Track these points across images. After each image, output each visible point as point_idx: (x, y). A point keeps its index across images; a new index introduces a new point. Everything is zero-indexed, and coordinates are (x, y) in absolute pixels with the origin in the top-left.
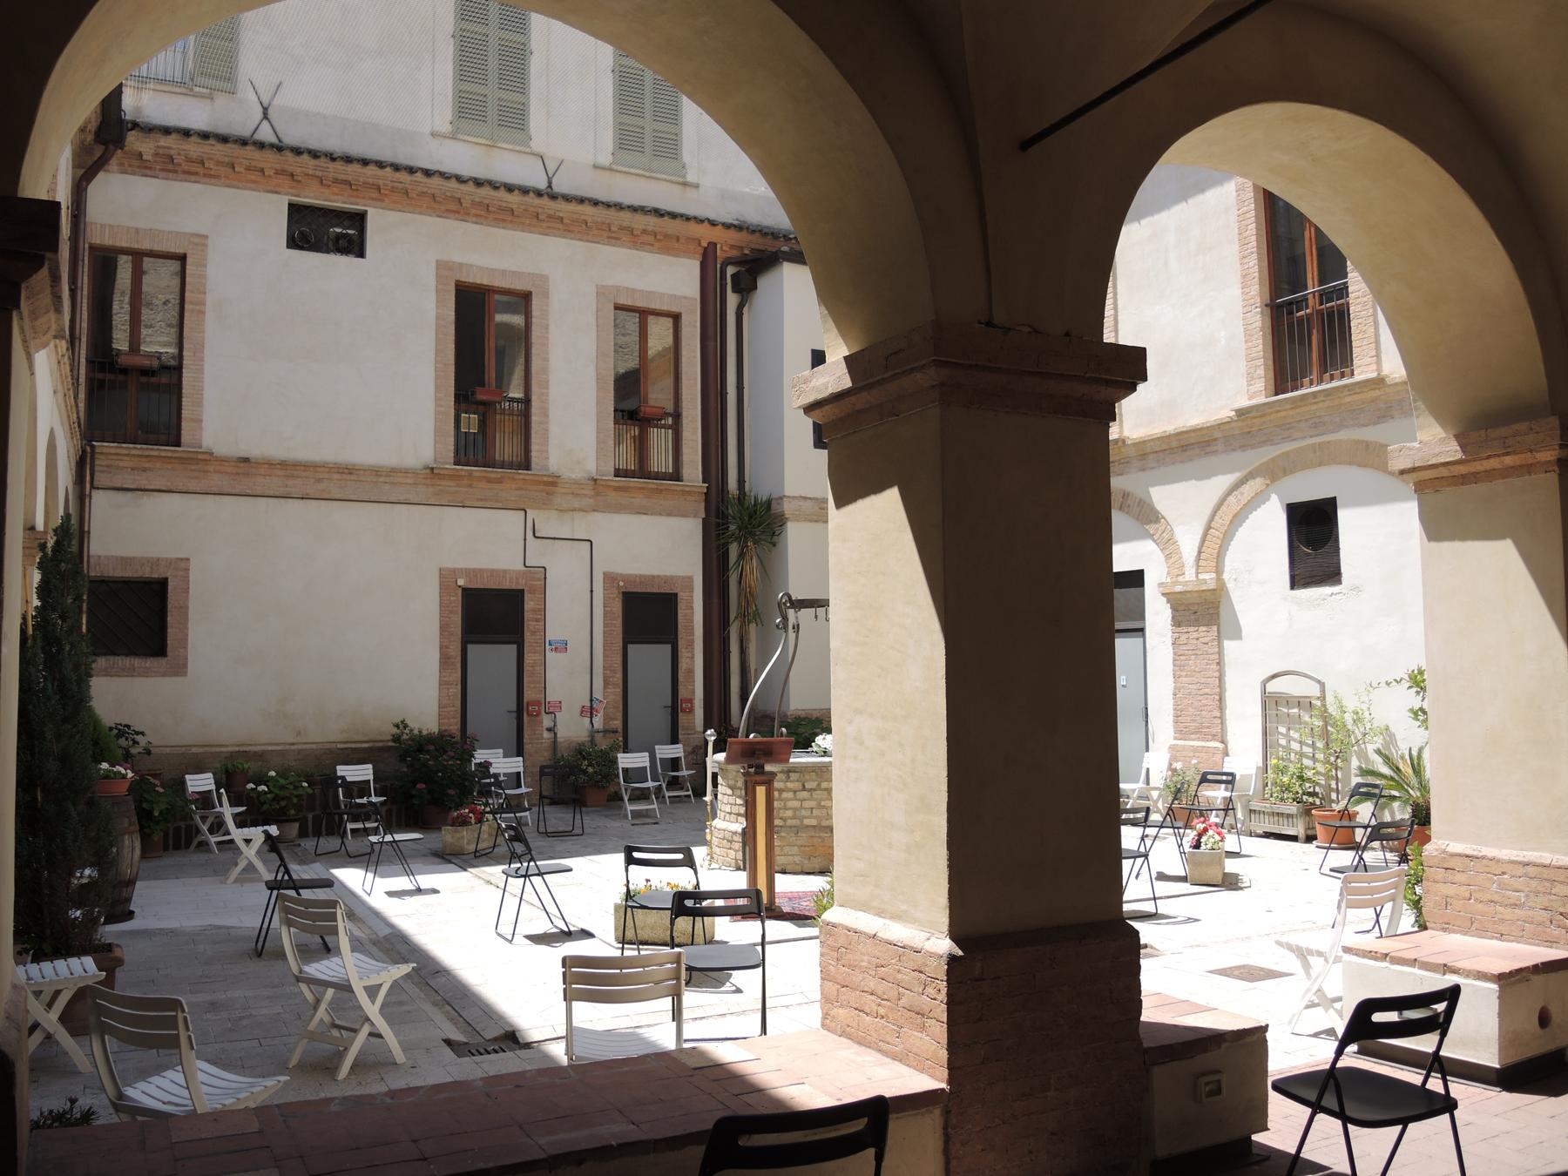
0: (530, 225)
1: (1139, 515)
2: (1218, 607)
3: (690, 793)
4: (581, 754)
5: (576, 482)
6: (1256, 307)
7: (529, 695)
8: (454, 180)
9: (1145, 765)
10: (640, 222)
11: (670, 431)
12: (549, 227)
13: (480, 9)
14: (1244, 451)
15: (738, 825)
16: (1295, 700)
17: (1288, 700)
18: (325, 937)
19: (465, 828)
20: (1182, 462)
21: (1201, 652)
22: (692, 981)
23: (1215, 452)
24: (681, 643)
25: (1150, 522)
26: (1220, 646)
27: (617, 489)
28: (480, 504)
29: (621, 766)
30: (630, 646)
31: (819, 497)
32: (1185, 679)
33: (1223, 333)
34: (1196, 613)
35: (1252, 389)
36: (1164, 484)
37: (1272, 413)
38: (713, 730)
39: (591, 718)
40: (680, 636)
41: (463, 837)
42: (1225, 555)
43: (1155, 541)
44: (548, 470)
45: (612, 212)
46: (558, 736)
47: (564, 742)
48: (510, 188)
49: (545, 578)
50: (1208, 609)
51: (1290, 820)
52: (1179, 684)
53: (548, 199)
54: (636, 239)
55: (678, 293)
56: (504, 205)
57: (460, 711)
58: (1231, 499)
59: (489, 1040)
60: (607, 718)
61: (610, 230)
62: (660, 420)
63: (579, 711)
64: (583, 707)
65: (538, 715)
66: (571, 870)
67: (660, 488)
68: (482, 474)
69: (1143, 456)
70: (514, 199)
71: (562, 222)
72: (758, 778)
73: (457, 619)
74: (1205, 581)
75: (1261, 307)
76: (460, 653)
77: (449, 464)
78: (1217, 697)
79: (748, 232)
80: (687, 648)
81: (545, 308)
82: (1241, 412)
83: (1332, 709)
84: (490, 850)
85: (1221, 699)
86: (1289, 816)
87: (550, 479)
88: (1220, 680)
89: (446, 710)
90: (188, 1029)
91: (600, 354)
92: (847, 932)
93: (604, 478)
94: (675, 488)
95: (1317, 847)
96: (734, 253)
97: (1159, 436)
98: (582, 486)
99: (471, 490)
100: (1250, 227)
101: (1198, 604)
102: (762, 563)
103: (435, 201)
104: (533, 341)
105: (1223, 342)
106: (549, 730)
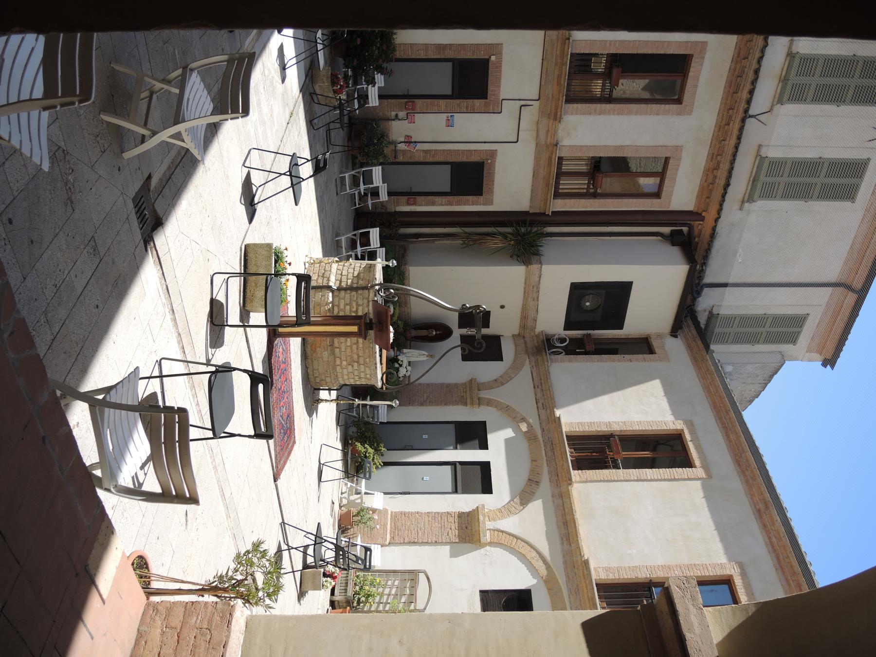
0: (726, 103)
1: (525, 492)
2: (470, 543)
3: (357, 206)
4: (381, 137)
5: (555, 133)
6: (650, 575)
7: (419, 102)
8: (761, 55)
9: (376, 493)
10: (722, 175)
11: (585, 191)
12: (723, 116)
13: (872, 70)
14: (563, 563)
15: (334, 281)
16: (415, 591)
17: (414, 587)
18: (140, 377)
19: (330, 84)
20: (557, 521)
22: (214, 326)
23: (562, 544)
24: (451, 198)
25: (521, 499)
26: (446, 543)
27: (550, 159)
28: (544, 70)
29: (371, 230)
30: (449, 166)
31: (540, 285)
32: (427, 520)
33: (634, 551)
35: (600, 570)
36: (544, 510)
37: (586, 583)
38: (396, 264)
39: (404, 142)
40: (455, 197)
41: (324, 83)
42: (501, 548)
43: (509, 502)
44: (564, 115)
45: (730, 157)
46: (393, 122)
47: (389, 125)
48: (751, 92)
49: (494, 113)
50: (469, 536)
51: (343, 591)
52: (424, 516)
53: (742, 116)
54: (711, 171)
55: (673, 197)
56: (741, 88)
57: (409, 57)
58: (534, 554)
59: (154, 206)
60: (404, 152)
61: (718, 155)
62: (593, 186)
63: (408, 134)
64: (411, 137)
65: (406, 109)
66: (296, 204)
67: (550, 185)
68: (564, 72)
69: (561, 496)
70: (745, 94)
71: (725, 125)
72: (363, 327)
73: (469, 55)
74: (485, 536)
75: (650, 577)
76: (447, 57)
77: (572, 51)
78: (416, 541)
79: (709, 241)
80: (448, 201)
81: (671, 113)
82: (586, 563)
84: (316, 101)
85: (415, 543)
86: (346, 590)
87: (558, 117)
88: (426, 542)
89: (409, 48)
90: (62, 105)
91: (637, 148)
92: (223, 644)
93: (558, 151)
94: (549, 194)
95: (328, 609)
96: (696, 232)
97: (573, 508)
98: (553, 137)
99: (554, 65)
100: (699, 572)
101: (472, 530)
102: (500, 250)
103: (748, 41)
104: (649, 105)
105: (629, 551)
106: (397, 115)
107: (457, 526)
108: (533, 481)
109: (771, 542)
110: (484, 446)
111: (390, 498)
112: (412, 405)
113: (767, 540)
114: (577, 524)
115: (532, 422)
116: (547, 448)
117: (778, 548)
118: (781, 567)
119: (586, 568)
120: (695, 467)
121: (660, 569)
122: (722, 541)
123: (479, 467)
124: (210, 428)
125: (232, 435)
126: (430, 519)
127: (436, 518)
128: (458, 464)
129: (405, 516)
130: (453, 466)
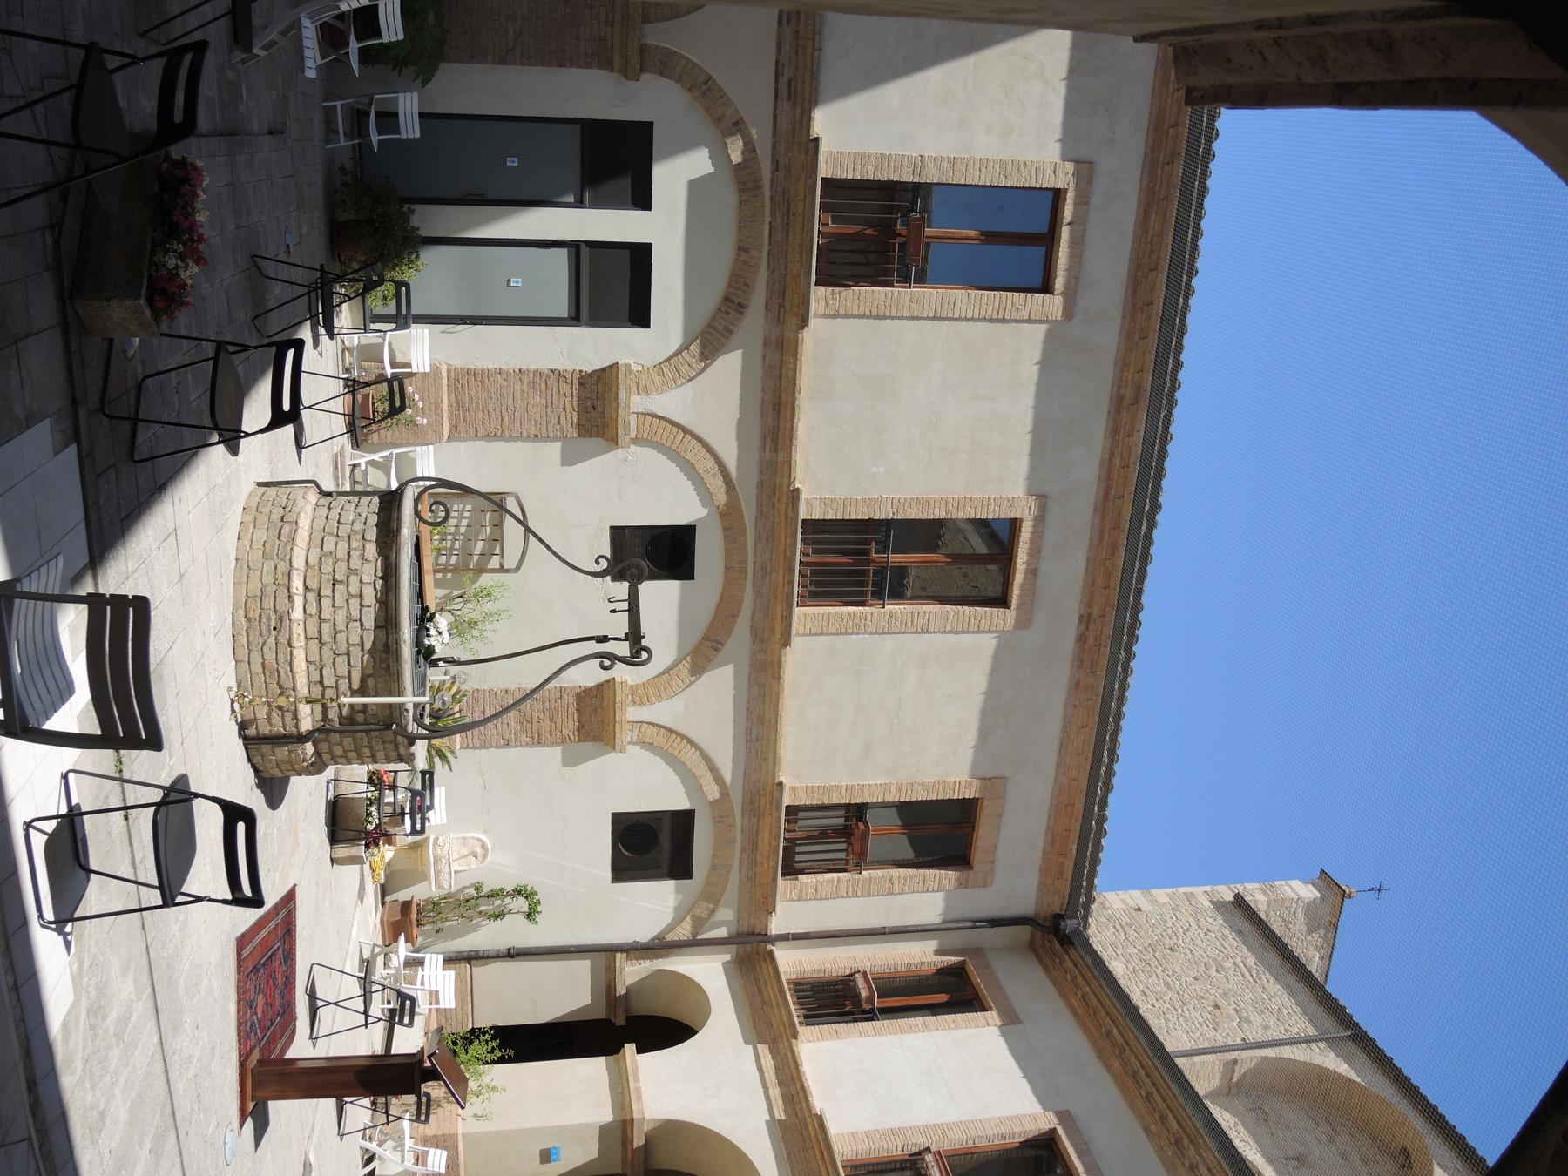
6: (894, 514)
14: (757, 486)
20: (763, 399)
21: (549, 413)
23: (763, 448)
25: (703, 346)
34: (594, 409)
36: (742, 374)
58: (711, 462)
83: (486, 580)
101: (603, 413)
107: (575, 403)
108: (733, 302)
109: (1110, 461)
110: (641, 199)
111: (443, 332)
112: (480, 62)
113: (1107, 457)
114: (796, 417)
115: (755, 137)
116: (775, 219)
117: (1116, 476)
118: (1104, 509)
119: (793, 508)
120: (1052, 293)
121: (914, 504)
122: (1032, 454)
123: (628, 252)
124: (156, 884)
125: (198, 899)
126: (525, 387)
127: (537, 386)
128: (583, 246)
129: (475, 380)
130: (573, 250)
